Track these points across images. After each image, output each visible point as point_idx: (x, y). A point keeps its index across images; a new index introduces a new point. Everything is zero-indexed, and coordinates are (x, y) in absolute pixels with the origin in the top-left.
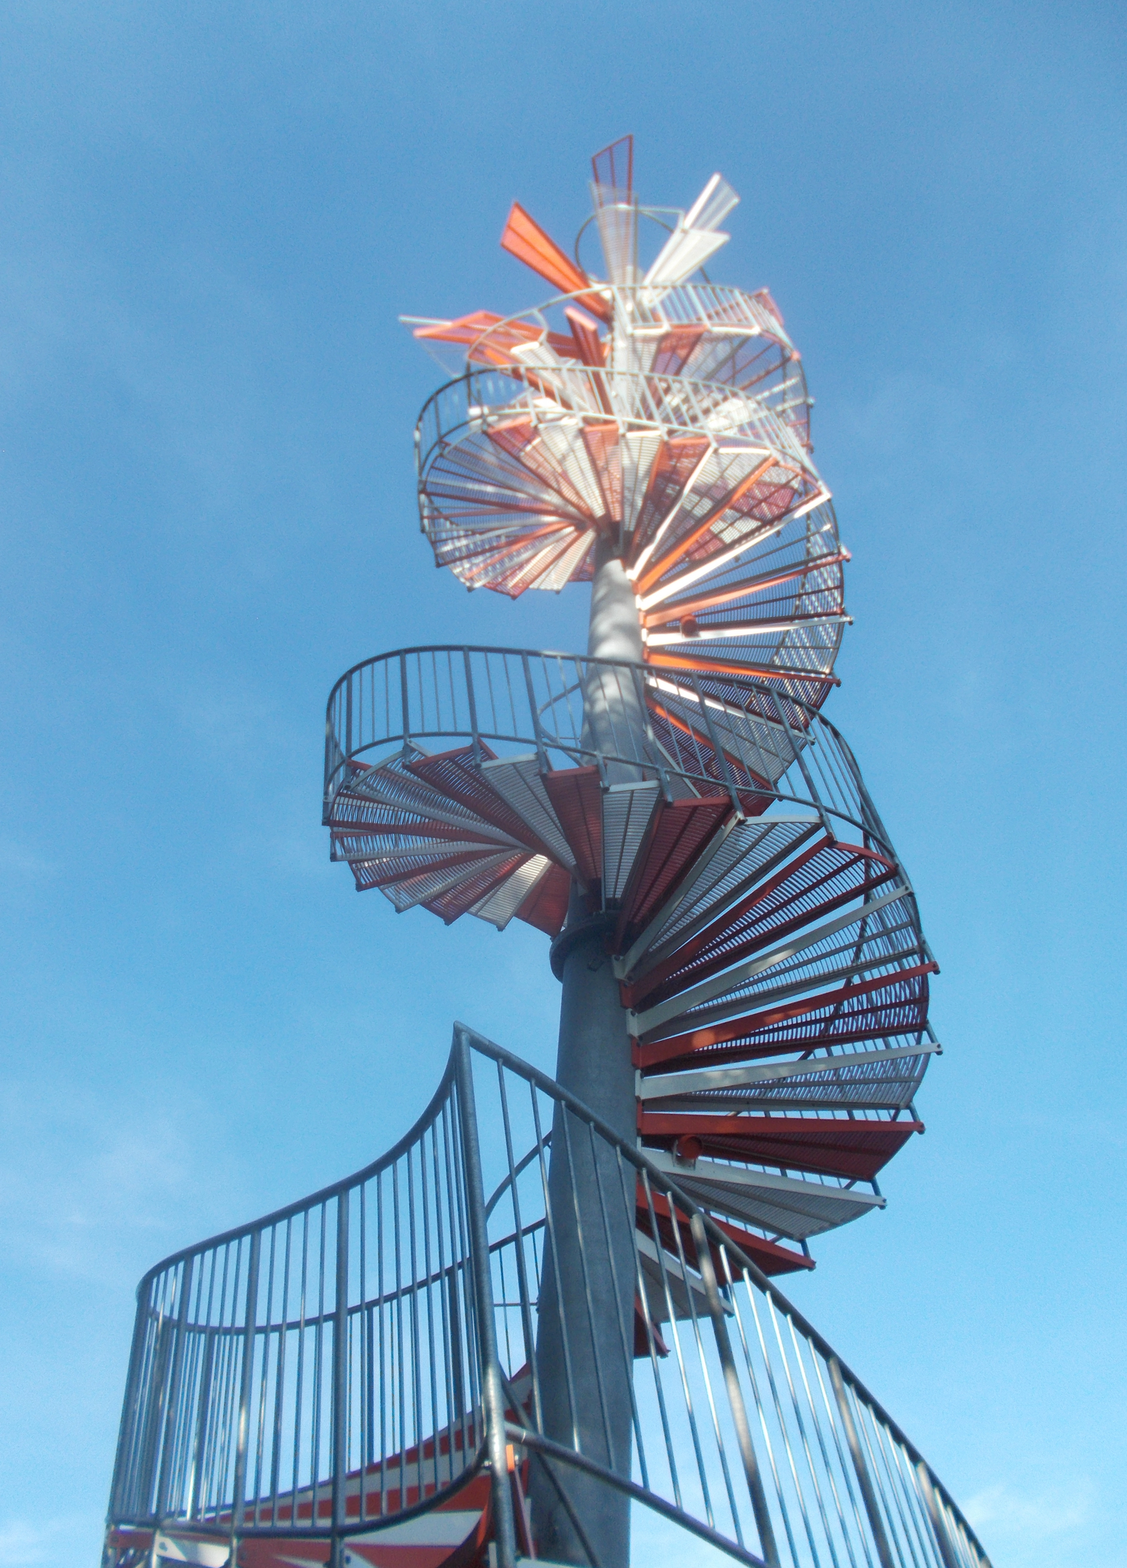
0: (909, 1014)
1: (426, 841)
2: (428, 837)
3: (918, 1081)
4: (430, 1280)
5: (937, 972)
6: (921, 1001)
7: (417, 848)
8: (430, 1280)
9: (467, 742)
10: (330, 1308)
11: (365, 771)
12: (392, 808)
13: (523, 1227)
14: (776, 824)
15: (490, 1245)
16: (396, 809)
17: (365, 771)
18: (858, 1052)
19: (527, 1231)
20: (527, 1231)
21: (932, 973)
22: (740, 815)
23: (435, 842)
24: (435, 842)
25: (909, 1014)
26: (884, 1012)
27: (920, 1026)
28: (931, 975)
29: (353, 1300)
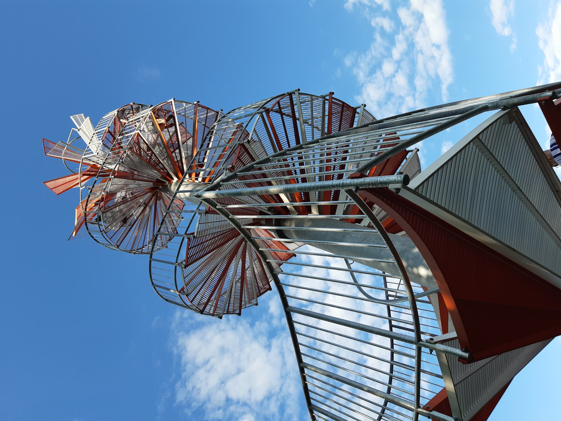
0: (347, 113)
1: (234, 262)
2: (232, 262)
3: (343, 103)
4: (392, 349)
5: (333, 93)
6: (344, 105)
7: (235, 266)
8: (392, 349)
9: (186, 240)
10: (386, 342)
11: (184, 288)
12: (222, 262)
13: (389, 347)
14: (254, 129)
15: (389, 330)
16: (222, 262)
17: (296, 175)
18: (350, 265)
19: (392, 347)
20: (392, 347)
21: (333, 95)
22: (81, 189)
23: (235, 259)
24: (235, 259)
25: (347, 113)
26: (332, 132)
27: (354, 110)
28: (333, 96)
29: (386, 327)
